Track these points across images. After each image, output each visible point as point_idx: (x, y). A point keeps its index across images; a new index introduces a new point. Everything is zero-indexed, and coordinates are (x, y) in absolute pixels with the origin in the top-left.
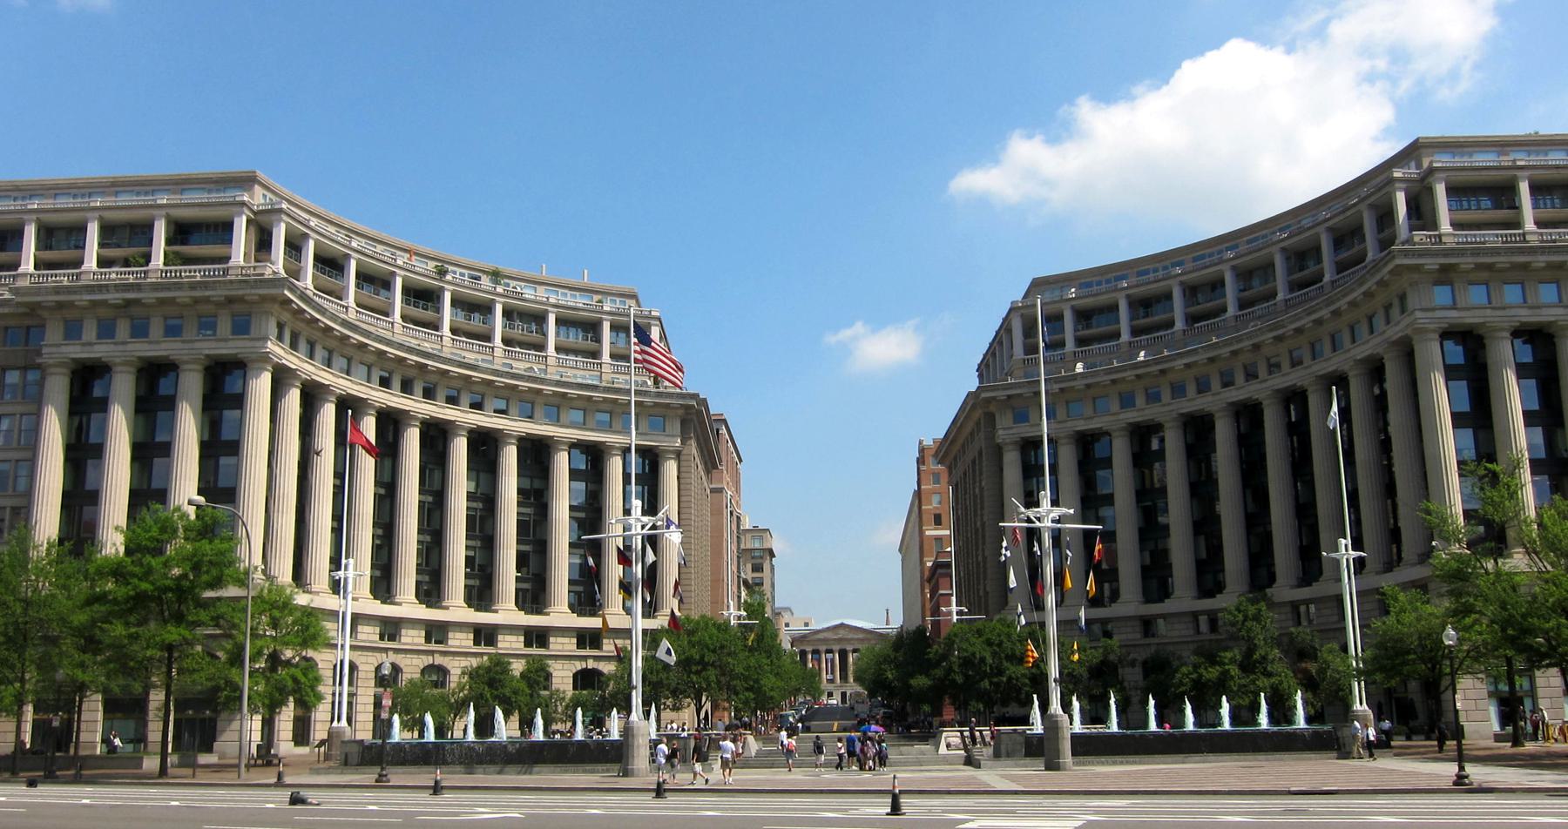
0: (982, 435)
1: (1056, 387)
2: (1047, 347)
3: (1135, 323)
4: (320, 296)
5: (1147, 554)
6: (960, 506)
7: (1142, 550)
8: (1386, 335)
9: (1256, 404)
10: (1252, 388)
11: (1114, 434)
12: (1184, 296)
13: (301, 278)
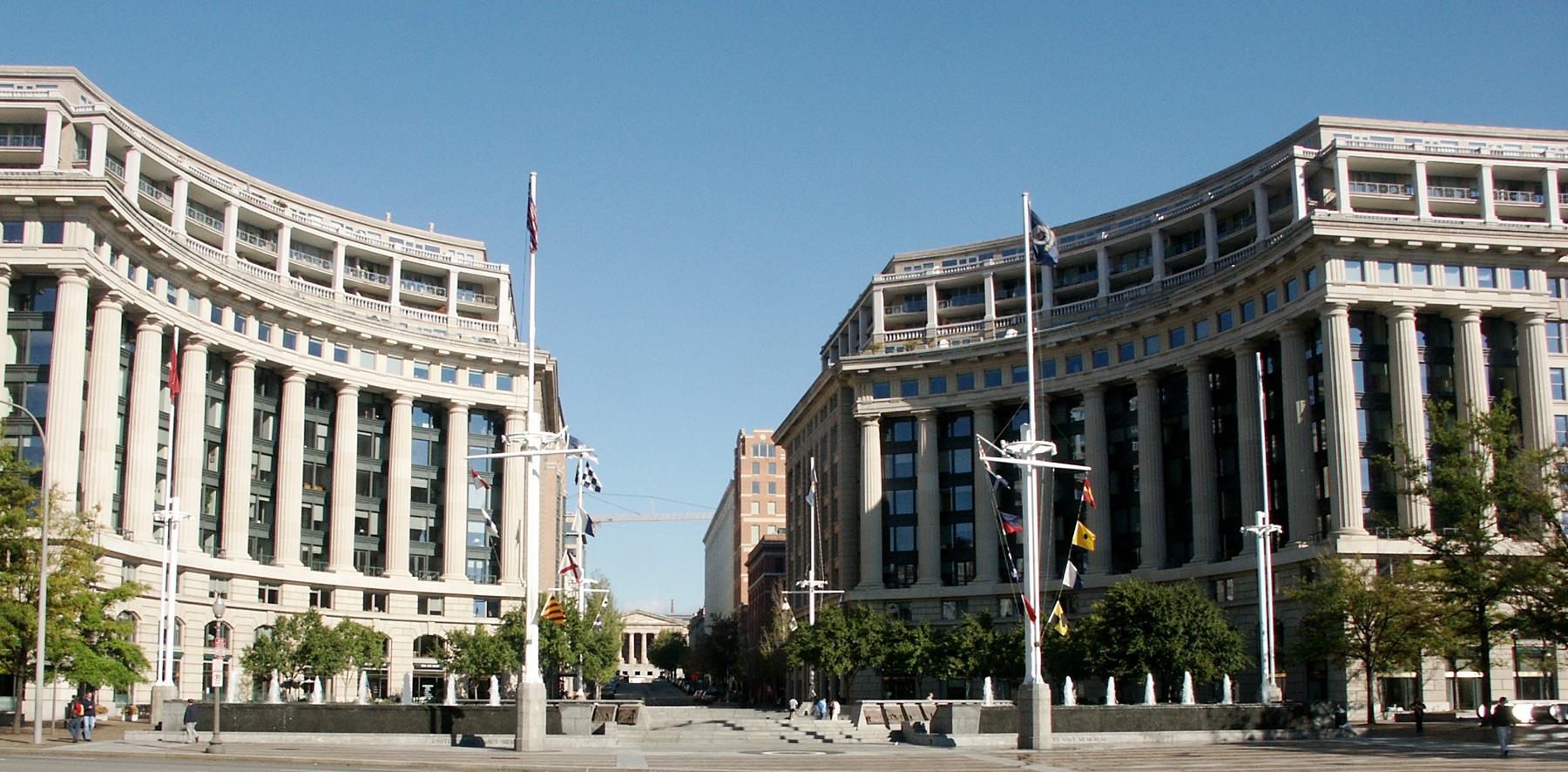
0: (838, 410)
8: (1286, 313)
10: (1127, 368)
11: (976, 412)
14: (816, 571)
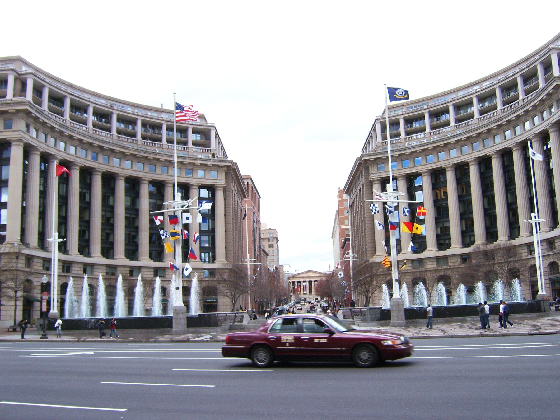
1: (397, 154)
2: (391, 137)
3: (432, 123)
4: (52, 115)
5: (439, 230)
6: (354, 212)
7: (436, 228)
9: (488, 158)
12: (455, 111)
13: (42, 107)
14: (353, 250)
